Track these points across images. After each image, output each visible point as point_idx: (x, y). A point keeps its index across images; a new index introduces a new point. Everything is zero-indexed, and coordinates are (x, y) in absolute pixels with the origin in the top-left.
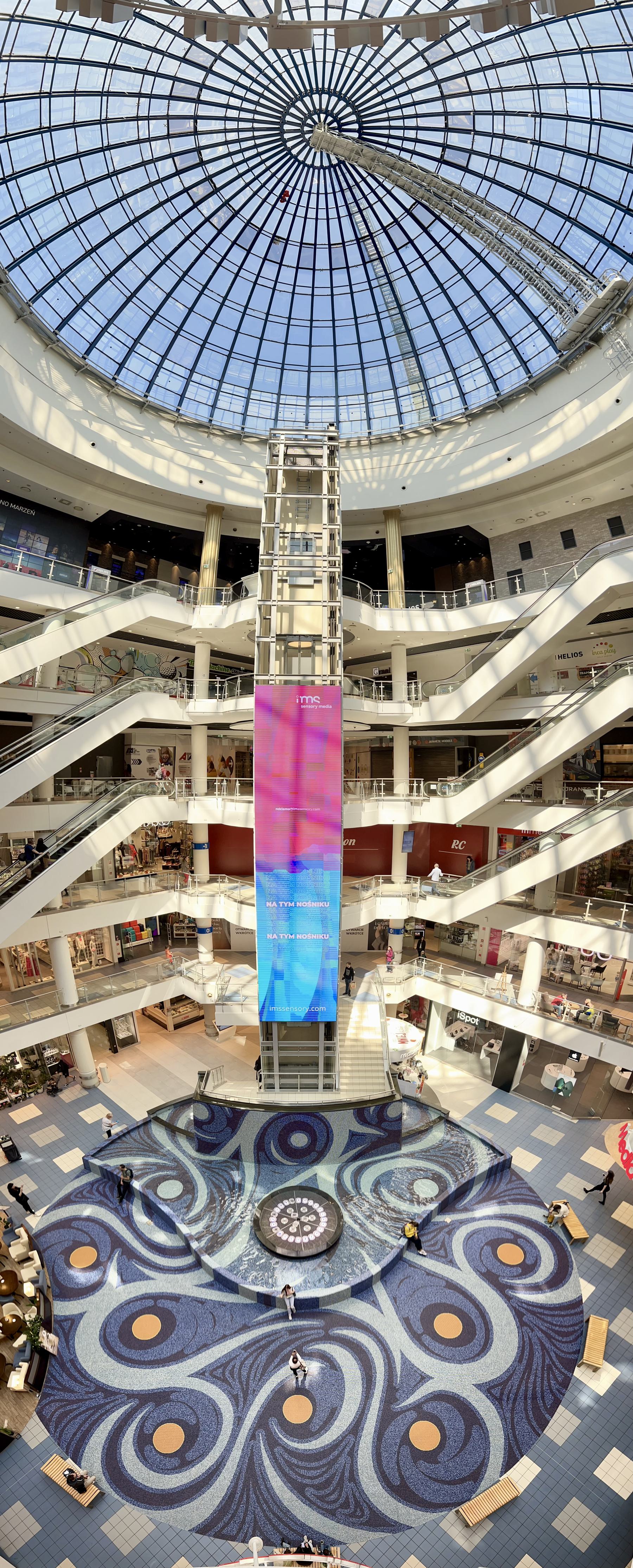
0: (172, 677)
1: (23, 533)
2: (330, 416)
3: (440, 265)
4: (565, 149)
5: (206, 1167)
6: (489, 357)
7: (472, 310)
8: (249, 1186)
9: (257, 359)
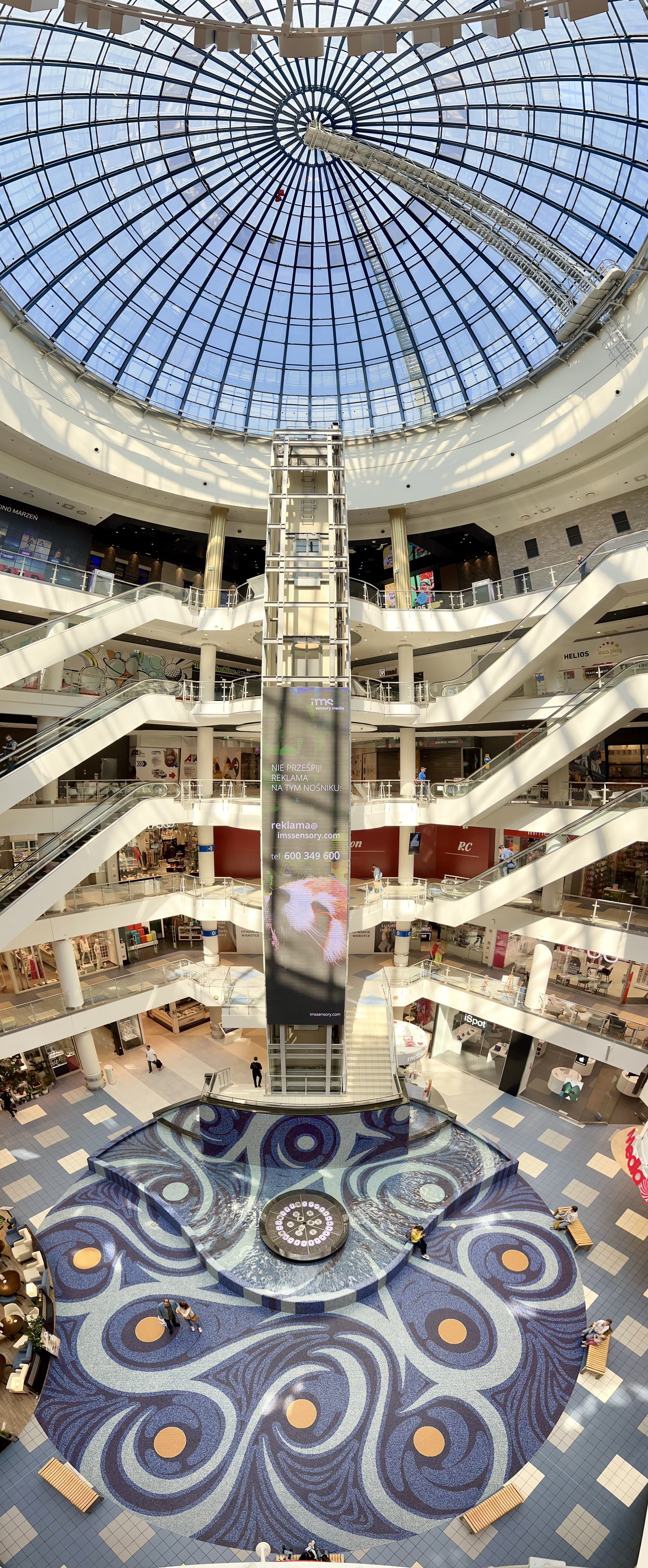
0: (177, 679)
1: (25, 538)
2: (333, 415)
3: (438, 259)
4: (560, 141)
5: (212, 1170)
6: (489, 351)
7: (471, 304)
8: (255, 1182)
9: (258, 360)
